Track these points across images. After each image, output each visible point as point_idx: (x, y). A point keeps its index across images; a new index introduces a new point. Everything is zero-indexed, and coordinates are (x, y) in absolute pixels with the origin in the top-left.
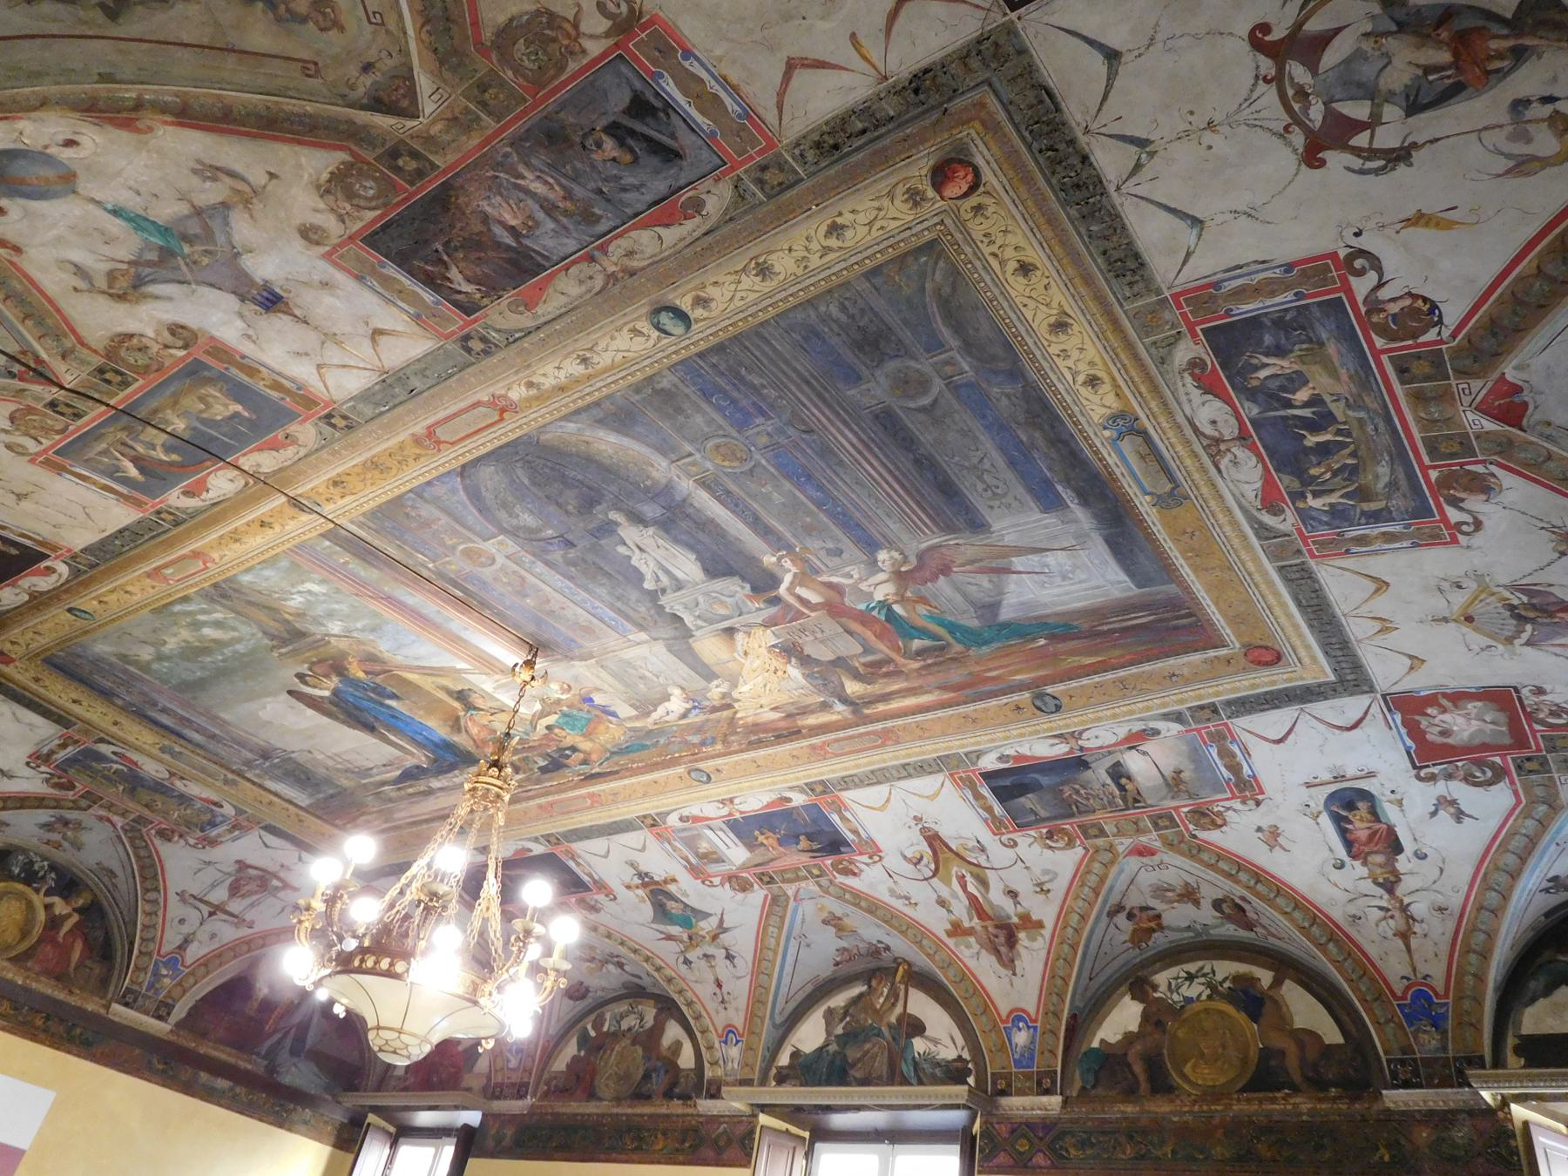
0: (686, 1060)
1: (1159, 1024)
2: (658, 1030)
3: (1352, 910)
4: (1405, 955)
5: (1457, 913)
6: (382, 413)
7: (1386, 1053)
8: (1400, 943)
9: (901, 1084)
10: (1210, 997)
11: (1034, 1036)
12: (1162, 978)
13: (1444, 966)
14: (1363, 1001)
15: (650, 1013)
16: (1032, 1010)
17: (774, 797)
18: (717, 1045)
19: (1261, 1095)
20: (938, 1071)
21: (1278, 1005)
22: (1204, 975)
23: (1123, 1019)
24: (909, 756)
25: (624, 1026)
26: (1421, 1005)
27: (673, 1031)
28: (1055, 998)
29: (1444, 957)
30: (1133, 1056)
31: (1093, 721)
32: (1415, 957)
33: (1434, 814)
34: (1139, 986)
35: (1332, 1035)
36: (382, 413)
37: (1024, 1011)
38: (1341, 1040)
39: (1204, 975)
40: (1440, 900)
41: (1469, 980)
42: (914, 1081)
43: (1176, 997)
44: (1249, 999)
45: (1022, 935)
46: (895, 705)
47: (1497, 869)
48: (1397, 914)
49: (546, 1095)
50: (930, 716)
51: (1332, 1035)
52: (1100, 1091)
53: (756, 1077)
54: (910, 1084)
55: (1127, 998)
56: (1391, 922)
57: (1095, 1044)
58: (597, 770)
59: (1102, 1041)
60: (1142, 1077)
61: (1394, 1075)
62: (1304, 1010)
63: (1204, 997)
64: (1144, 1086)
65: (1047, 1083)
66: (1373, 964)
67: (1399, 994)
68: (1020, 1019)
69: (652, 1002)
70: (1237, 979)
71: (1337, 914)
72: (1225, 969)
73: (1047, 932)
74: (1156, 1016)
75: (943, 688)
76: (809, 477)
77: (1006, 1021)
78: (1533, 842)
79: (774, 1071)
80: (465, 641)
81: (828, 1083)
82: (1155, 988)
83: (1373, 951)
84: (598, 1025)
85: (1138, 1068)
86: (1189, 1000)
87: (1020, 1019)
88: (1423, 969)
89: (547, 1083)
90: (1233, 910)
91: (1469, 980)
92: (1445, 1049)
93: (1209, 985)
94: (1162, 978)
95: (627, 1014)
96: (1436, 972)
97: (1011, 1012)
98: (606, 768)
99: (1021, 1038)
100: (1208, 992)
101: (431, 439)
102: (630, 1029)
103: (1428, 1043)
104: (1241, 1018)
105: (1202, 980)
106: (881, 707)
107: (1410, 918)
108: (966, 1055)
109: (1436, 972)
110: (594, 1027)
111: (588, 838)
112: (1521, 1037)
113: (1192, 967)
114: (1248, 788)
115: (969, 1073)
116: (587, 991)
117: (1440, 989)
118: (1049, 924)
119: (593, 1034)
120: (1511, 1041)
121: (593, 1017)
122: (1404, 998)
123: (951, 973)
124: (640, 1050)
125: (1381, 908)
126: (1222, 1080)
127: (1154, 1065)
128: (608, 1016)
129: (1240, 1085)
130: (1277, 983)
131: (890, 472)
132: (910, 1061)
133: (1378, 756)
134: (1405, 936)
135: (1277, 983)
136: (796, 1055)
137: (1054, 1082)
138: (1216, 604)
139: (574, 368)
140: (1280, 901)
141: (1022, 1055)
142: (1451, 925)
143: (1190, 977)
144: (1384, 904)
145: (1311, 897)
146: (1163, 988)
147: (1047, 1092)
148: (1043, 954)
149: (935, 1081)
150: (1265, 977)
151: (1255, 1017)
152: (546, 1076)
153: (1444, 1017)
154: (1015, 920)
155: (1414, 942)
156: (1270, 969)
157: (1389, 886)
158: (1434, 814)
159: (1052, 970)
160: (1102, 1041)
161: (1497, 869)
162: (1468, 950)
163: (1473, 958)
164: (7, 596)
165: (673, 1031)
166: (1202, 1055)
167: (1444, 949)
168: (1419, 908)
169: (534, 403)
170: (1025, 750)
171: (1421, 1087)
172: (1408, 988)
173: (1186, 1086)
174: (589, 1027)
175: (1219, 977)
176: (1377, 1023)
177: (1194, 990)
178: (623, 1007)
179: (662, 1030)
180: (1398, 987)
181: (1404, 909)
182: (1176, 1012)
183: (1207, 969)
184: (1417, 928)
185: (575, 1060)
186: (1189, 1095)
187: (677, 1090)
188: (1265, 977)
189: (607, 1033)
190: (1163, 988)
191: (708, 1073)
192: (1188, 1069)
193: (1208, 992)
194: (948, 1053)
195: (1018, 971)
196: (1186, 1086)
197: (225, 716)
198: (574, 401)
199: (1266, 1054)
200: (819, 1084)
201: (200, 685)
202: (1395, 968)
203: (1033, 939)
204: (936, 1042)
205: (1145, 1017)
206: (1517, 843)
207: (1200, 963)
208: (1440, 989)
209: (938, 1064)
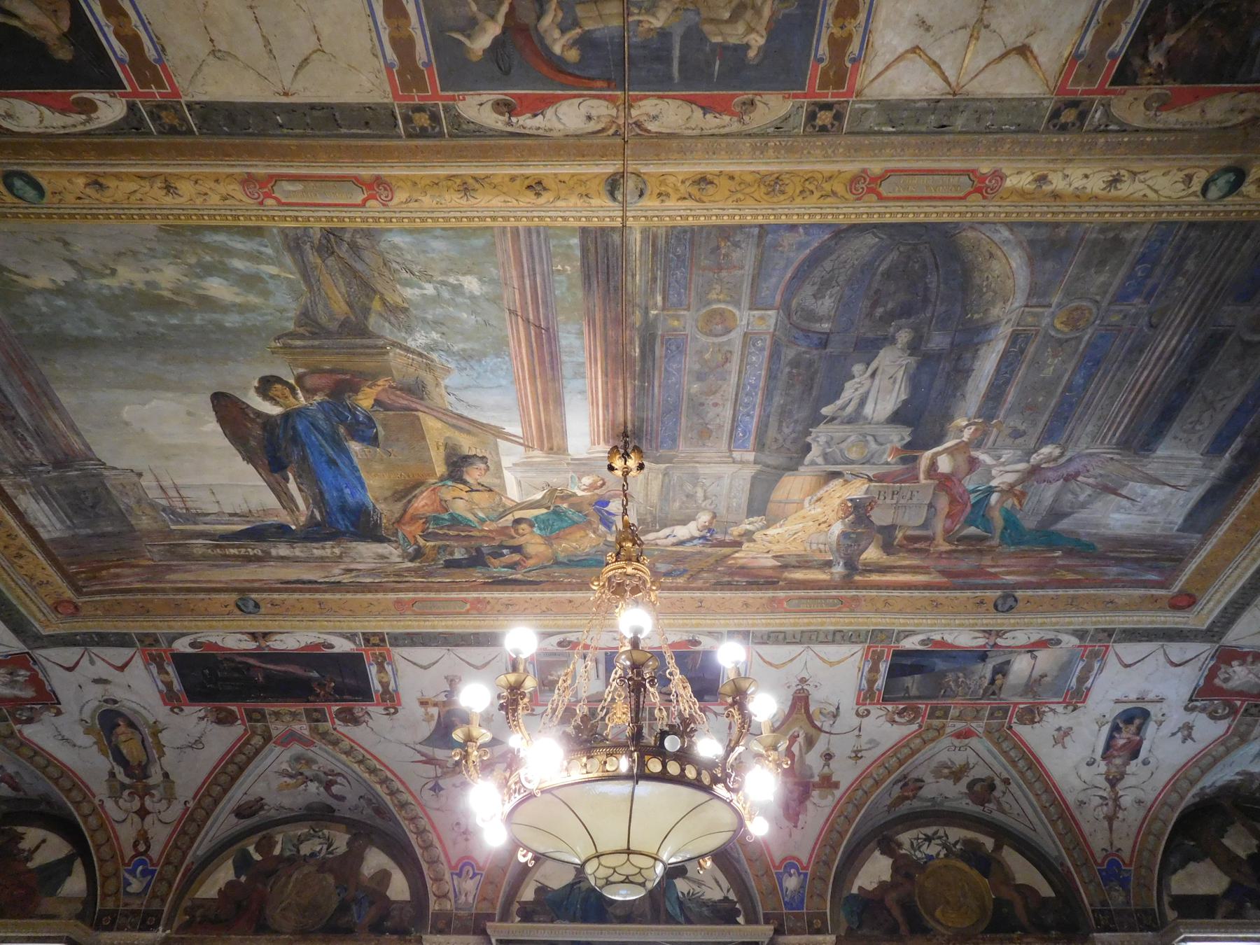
0: (399, 888)
1: (909, 876)
2: (354, 857)
3: (1082, 797)
4: (1108, 832)
5: (1149, 805)
6: (880, 133)
7: (1091, 905)
8: (1106, 824)
9: (667, 922)
10: (946, 856)
11: (805, 880)
12: (905, 838)
13: (1131, 842)
14: (1075, 866)
15: (341, 841)
16: (805, 861)
17: (685, 637)
18: (447, 877)
19: (1001, 935)
20: (705, 911)
21: (1001, 864)
22: (940, 838)
23: (875, 871)
24: (753, 625)
25: (305, 849)
26: (1113, 871)
27: (375, 860)
28: (828, 850)
29: (1133, 837)
30: (891, 899)
31: (1014, 625)
32: (1114, 835)
33: (1173, 734)
34: (888, 847)
35: (1046, 891)
36: (880, 133)
37: (798, 860)
38: (1053, 895)
39: (940, 838)
40: (1141, 795)
41: (1146, 854)
42: (682, 919)
43: (919, 854)
44: (984, 863)
45: (815, 793)
46: (889, 578)
47: (1186, 778)
48: (1110, 803)
49: (185, 927)
50: (896, 593)
51: (1046, 891)
52: (865, 931)
53: (497, 912)
54: (678, 923)
55: (877, 853)
56: (1105, 808)
57: (855, 891)
58: (519, 576)
59: (860, 888)
60: (900, 919)
61: (1098, 922)
62: (1023, 871)
63: (942, 855)
64: (903, 929)
65: (818, 923)
66: (1085, 839)
67: (1099, 861)
68: (793, 866)
69: (343, 827)
70: (967, 842)
71: (1071, 799)
72: (956, 834)
73: (838, 793)
74: (904, 869)
75: (943, 573)
76: (1098, 363)
77: (779, 867)
78: (1216, 761)
79: (516, 906)
80: (559, 402)
81: (585, 920)
82: (900, 845)
83: (1086, 828)
84: (265, 846)
85: (896, 912)
86: (930, 858)
87: (793, 866)
88: (1117, 844)
89: (189, 911)
90: (984, 790)
91: (1146, 854)
92: (1128, 903)
93: (944, 846)
94: (905, 838)
95: (308, 837)
96: (1126, 846)
97: (785, 859)
98: (532, 577)
99: (791, 883)
100: (944, 851)
101: (865, 185)
102: (313, 855)
103: (1117, 898)
104: (974, 874)
105: (939, 841)
106: (875, 577)
107: (1118, 806)
108: (732, 896)
109: (1126, 846)
110: (257, 850)
111: (424, 645)
112: (1171, 896)
113: (929, 831)
114: (47, 699)
115: (738, 913)
116: (262, 808)
117: (1127, 861)
118: (843, 787)
119: (257, 857)
120: (1166, 899)
121: (256, 838)
122: (1102, 864)
123: (93, 821)
124: (331, 879)
125: (1101, 797)
126: (967, 923)
127: (908, 908)
128: (279, 838)
129: (982, 928)
130: (998, 847)
131: (1154, 383)
132: (674, 899)
133: (140, 688)
134: (1110, 819)
135: (998, 847)
136: (541, 890)
137: (824, 922)
138: (1207, 556)
139: (1096, 184)
140: (1037, 785)
141: (792, 898)
142: (1142, 813)
143: (929, 839)
144: (1105, 795)
145: (1060, 786)
146: (907, 845)
147: (819, 932)
148: (827, 811)
149: (704, 920)
150: (989, 843)
151: (985, 873)
152: (186, 903)
153: (1127, 880)
154: (816, 779)
155: (1116, 824)
156: (991, 836)
157: (1113, 781)
158: (1173, 734)
159: (832, 825)
160: (860, 888)
161: (1186, 778)
162: (1149, 833)
163: (1151, 838)
164: (29, 116)
165: (375, 860)
166: (948, 903)
167: (1134, 830)
168: (1126, 801)
169: (1015, 198)
170: (949, 639)
171: (1116, 931)
172: (1106, 857)
173: (939, 928)
174: (251, 849)
175: (952, 840)
176: (1083, 882)
177: (933, 849)
178: (303, 830)
179: (361, 859)
180: (1099, 856)
181: (1116, 799)
182: (921, 866)
183: (941, 833)
184: (1120, 815)
185: (230, 884)
186: (943, 935)
187: (388, 924)
188: (989, 843)
189: (280, 858)
190: (907, 845)
191: (434, 906)
192: (938, 913)
193: (944, 851)
194: (714, 894)
195: (800, 824)
196: (939, 928)
197: (66, 398)
198: (1043, 214)
199: (998, 903)
200: (573, 920)
201: (56, 342)
202: (1098, 842)
203: (823, 797)
204: (700, 883)
205: (895, 869)
206: (1205, 762)
207: (935, 828)
208: (1127, 861)
209: (705, 904)
